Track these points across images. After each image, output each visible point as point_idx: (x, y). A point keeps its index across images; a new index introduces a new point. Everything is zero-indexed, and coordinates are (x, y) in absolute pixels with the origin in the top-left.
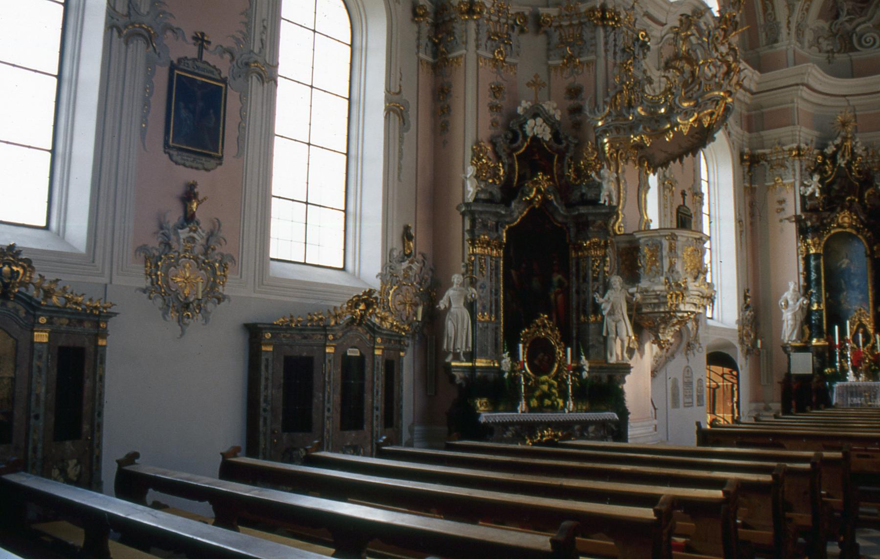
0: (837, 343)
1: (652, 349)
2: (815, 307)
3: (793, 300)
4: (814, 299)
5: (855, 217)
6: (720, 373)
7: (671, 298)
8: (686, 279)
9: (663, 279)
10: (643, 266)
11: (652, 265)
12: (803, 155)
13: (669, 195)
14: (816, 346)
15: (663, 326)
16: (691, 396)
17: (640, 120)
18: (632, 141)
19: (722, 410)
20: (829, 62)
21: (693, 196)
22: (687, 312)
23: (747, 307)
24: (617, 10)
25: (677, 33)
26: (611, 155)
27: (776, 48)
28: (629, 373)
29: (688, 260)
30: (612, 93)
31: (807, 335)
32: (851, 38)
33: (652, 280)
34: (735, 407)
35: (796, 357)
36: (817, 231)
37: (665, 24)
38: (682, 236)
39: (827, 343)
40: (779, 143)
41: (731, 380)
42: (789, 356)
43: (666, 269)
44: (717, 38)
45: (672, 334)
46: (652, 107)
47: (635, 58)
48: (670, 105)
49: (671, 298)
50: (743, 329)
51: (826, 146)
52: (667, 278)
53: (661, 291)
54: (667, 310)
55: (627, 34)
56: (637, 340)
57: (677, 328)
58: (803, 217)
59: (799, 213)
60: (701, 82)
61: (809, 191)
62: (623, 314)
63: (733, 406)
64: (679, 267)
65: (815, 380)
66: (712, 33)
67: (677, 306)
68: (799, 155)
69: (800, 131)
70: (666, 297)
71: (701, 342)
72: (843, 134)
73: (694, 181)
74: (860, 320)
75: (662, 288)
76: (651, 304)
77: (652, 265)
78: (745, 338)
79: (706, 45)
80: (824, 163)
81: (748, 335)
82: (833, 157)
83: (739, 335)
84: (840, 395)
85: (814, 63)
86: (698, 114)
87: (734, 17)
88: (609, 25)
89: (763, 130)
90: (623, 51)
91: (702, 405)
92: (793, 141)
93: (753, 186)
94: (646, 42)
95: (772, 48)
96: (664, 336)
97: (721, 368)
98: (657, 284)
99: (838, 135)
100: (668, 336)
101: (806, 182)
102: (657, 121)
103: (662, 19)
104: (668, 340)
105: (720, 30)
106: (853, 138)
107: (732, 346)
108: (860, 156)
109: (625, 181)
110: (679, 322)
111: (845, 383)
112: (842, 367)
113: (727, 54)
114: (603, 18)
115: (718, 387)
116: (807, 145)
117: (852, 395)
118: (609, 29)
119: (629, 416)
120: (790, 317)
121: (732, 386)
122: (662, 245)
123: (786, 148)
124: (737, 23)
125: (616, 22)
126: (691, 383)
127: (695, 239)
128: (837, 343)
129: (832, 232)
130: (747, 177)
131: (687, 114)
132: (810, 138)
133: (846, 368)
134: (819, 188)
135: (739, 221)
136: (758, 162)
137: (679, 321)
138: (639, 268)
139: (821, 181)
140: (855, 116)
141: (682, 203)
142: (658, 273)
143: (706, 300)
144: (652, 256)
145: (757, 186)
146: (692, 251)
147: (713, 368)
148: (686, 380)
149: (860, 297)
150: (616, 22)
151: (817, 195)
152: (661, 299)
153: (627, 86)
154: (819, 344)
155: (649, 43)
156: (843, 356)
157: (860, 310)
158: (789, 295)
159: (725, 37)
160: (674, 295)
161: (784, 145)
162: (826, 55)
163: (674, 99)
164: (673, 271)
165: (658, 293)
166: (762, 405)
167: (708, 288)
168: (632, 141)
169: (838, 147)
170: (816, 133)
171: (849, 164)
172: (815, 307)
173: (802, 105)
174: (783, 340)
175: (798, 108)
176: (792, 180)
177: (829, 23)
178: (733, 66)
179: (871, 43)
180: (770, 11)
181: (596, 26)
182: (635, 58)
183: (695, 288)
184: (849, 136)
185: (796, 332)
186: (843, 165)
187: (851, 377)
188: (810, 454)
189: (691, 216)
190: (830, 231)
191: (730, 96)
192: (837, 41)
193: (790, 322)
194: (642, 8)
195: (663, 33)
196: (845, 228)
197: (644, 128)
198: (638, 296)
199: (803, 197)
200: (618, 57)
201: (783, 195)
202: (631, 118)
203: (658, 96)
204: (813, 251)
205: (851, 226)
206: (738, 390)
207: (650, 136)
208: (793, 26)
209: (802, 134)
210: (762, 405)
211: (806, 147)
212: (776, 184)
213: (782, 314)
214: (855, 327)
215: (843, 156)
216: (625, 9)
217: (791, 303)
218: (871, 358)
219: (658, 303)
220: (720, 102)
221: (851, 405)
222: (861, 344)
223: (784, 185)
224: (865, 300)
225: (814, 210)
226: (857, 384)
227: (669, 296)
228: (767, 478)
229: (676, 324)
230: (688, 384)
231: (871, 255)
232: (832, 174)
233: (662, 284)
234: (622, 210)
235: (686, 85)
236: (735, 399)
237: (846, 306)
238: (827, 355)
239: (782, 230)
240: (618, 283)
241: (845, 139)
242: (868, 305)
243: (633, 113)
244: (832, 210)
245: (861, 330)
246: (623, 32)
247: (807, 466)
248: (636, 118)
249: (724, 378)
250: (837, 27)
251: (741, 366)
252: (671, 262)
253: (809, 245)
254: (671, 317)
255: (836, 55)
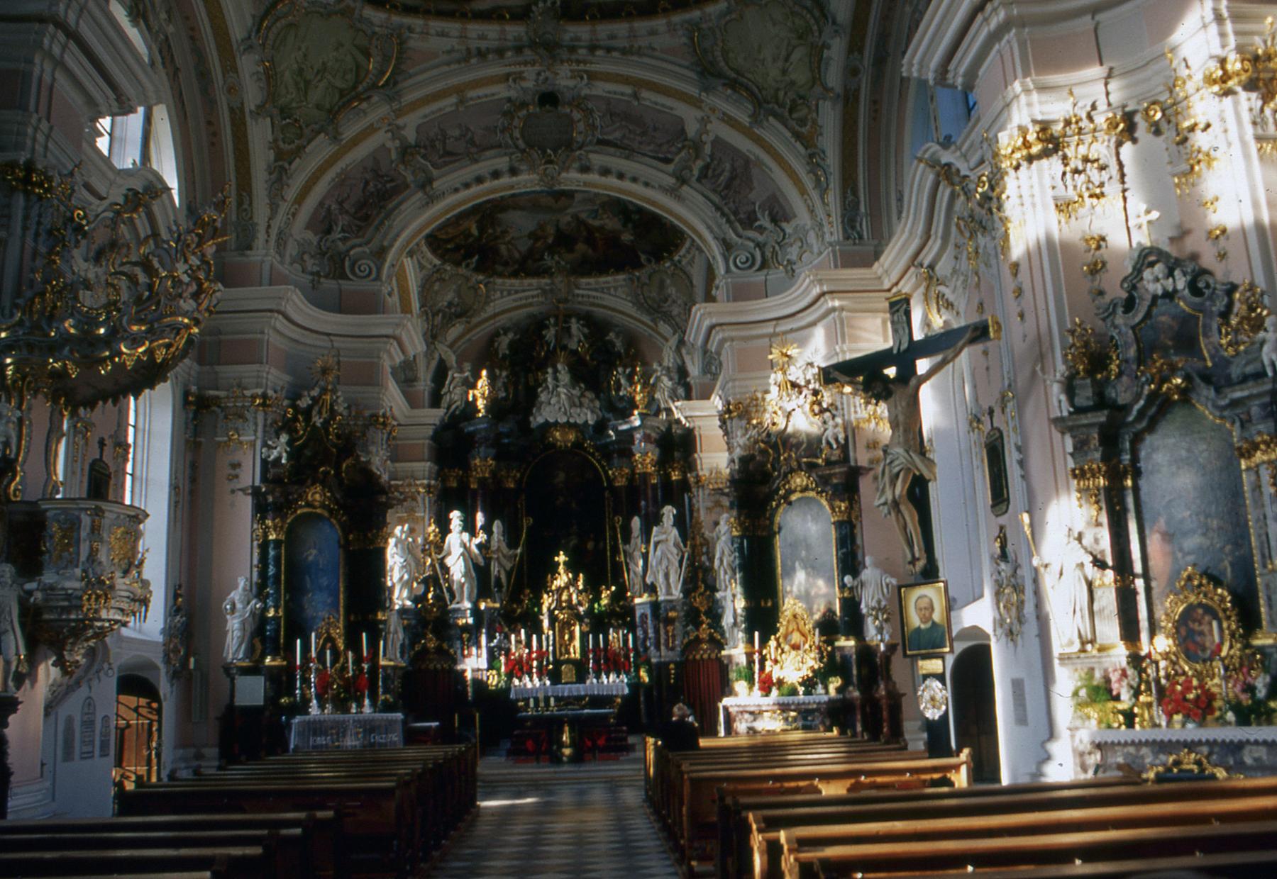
0: (298, 662)
1: (48, 675)
2: (271, 613)
3: (242, 602)
4: (270, 603)
5: (328, 494)
6: (134, 705)
7: (89, 600)
8: (112, 573)
9: (78, 572)
10: (48, 551)
11: (62, 551)
12: (269, 406)
13: (82, 443)
14: (270, 667)
15: (71, 641)
16: (92, 742)
17: (66, 339)
18: (50, 367)
19: (134, 761)
20: (313, 287)
21: (115, 447)
22: (109, 621)
23: (178, 611)
24: (50, 174)
25: (118, 213)
26: (14, 382)
27: (247, 256)
28: (15, 711)
29: (117, 547)
30: (29, 294)
31: (258, 652)
32: (343, 261)
33: (61, 572)
34: (153, 756)
35: (243, 683)
36: (279, 510)
37: (105, 198)
38: (111, 511)
39: (285, 663)
40: (239, 386)
41: (150, 716)
42: (232, 680)
43: (83, 558)
44: (188, 246)
45: (82, 651)
46: (86, 324)
47: (64, 246)
48: (114, 326)
49: (89, 600)
50: (170, 641)
51: (299, 397)
52: (84, 571)
53: (75, 590)
54: (81, 617)
55: (58, 210)
56: (27, 661)
57: (91, 643)
58: (264, 490)
59: (257, 483)
60: (160, 301)
61: (275, 454)
62: (12, 622)
63: (150, 755)
64: (103, 557)
65: (267, 713)
66: (182, 238)
67: (97, 611)
68: (263, 405)
69: (268, 373)
70: (81, 598)
71: (111, 661)
72: (322, 383)
73: (119, 425)
74: (327, 632)
75: (77, 585)
76: (56, 607)
77: (62, 551)
78: (172, 655)
79: (173, 252)
80: (295, 419)
81: (176, 651)
82: (307, 413)
83: (164, 650)
84: (300, 734)
85: (296, 287)
86: (150, 343)
87: (214, 221)
88: (34, 193)
89: (219, 364)
90: (50, 233)
91: (107, 755)
92: (258, 385)
93: (198, 439)
94: (83, 226)
95: (243, 255)
96: (71, 655)
97: (136, 698)
98: (69, 579)
99: (315, 385)
100: (78, 655)
101: (270, 443)
102: (91, 344)
103: (103, 191)
104: (77, 661)
105: (193, 235)
106: (334, 391)
107: (153, 667)
108: (341, 415)
109: (31, 422)
110: (96, 636)
111: (307, 718)
112: (303, 695)
113: (199, 268)
114: (27, 180)
115: (128, 726)
116: (275, 392)
117: (315, 734)
118: (34, 198)
119: (12, 779)
120: (236, 626)
121: (150, 726)
122: (80, 521)
123: (248, 393)
124: (216, 229)
125: (46, 191)
126: (92, 723)
127: (129, 516)
128: (298, 662)
129: (299, 512)
130: (191, 427)
131: (135, 341)
132: (281, 383)
133: (309, 696)
134: (286, 452)
135: (174, 488)
136: (208, 407)
137: (95, 633)
138: (42, 553)
139: (289, 443)
140: (339, 363)
141: (98, 457)
142: (71, 562)
143: (137, 604)
144: (64, 537)
145: (202, 440)
146: (123, 533)
147: (123, 698)
148: (85, 718)
149: (329, 601)
150: (46, 191)
151: (284, 461)
152: (74, 602)
153: (53, 287)
154: (273, 663)
155: (86, 228)
156: (306, 681)
157: (329, 618)
158: (236, 595)
159: (199, 245)
160: (94, 596)
161: (246, 389)
162: (311, 277)
163: (120, 319)
164: (93, 561)
165: (70, 592)
166: (193, 750)
167: (142, 588)
168: (50, 367)
169: (315, 400)
170: (287, 378)
171: (326, 423)
172: (271, 613)
173: (273, 338)
174: (226, 658)
175: (268, 341)
176: (253, 438)
177: (318, 237)
178: (206, 285)
179: (367, 272)
180: (245, 206)
181: (13, 190)
182: (64, 246)
183: (124, 587)
184: (330, 387)
185: (243, 647)
186: (318, 424)
187: (314, 709)
188: (301, 815)
189: (109, 476)
190: (295, 511)
191: (196, 325)
192: (326, 262)
193: (237, 634)
194: (83, 175)
195: (100, 210)
196: (315, 507)
197: (71, 351)
198: (39, 595)
199: (264, 462)
200: (41, 239)
201: (238, 457)
202: (53, 334)
203: (96, 310)
204: (272, 537)
205: (323, 506)
206: (159, 730)
207: (77, 364)
208: (274, 232)
209: (270, 377)
210: (193, 750)
211: (274, 396)
212: (230, 440)
213: (226, 621)
214: (321, 642)
215: (320, 413)
216: (60, 174)
217: (239, 606)
218: (341, 683)
219: (68, 606)
220: (183, 331)
221: (314, 747)
222: (328, 665)
223: (241, 443)
224: (335, 605)
225: (277, 481)
226: (322, 718)
227: (85, 597)
228: (256, 851)
229: (92, 637)
230: (89, 724)
231: (345, 546)
232: (303, 435)
233: (77, 580)
234: (22, 466)
235: (139, 301)
236: (154, 744)
237: (309, 612)
238: (284, 678)
239: (232, 505)
240: (8, 575)
241: (324, 391)
242: (338, 611)
243: (57, 328)
244: (302, 483)
245: (329, 645)
246: (52, 206)
247: (298, 831)
248: (61, 335)
249: (139, 714)
250: (328, 244)
251: (165, 695)
252: (91, 548)
253: (267, 527)
254: (86, 628)
255: (322, 280)
